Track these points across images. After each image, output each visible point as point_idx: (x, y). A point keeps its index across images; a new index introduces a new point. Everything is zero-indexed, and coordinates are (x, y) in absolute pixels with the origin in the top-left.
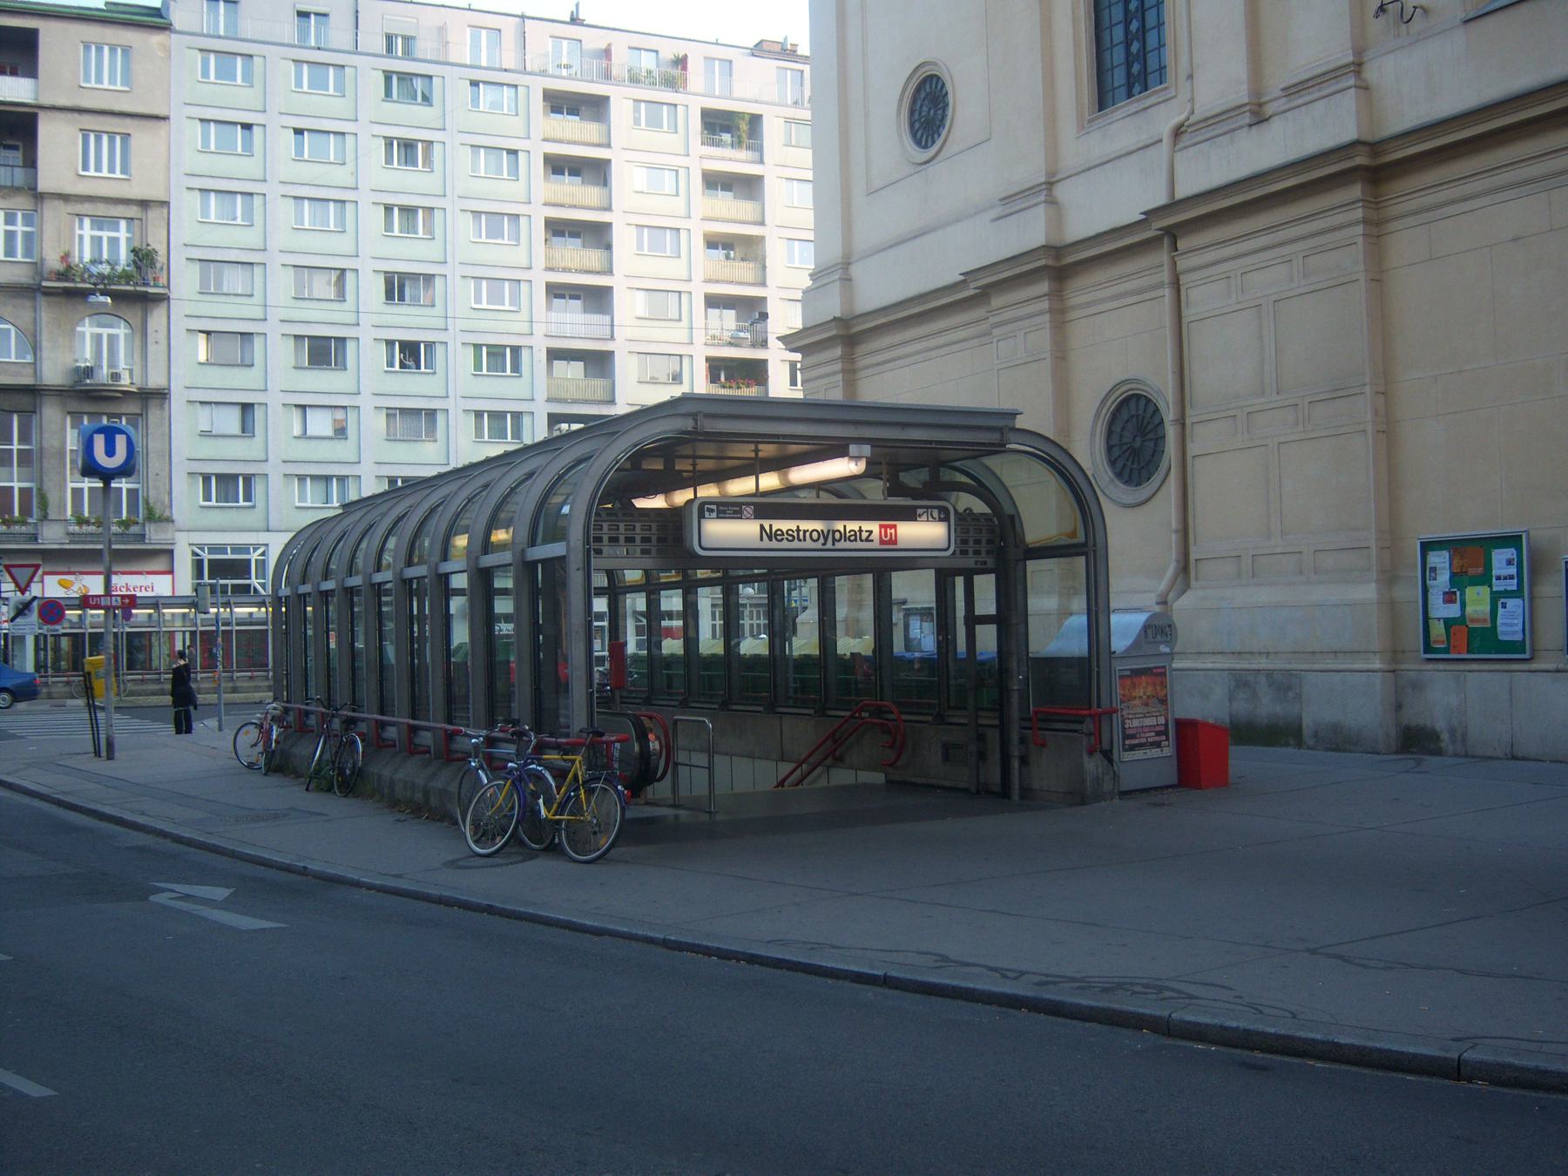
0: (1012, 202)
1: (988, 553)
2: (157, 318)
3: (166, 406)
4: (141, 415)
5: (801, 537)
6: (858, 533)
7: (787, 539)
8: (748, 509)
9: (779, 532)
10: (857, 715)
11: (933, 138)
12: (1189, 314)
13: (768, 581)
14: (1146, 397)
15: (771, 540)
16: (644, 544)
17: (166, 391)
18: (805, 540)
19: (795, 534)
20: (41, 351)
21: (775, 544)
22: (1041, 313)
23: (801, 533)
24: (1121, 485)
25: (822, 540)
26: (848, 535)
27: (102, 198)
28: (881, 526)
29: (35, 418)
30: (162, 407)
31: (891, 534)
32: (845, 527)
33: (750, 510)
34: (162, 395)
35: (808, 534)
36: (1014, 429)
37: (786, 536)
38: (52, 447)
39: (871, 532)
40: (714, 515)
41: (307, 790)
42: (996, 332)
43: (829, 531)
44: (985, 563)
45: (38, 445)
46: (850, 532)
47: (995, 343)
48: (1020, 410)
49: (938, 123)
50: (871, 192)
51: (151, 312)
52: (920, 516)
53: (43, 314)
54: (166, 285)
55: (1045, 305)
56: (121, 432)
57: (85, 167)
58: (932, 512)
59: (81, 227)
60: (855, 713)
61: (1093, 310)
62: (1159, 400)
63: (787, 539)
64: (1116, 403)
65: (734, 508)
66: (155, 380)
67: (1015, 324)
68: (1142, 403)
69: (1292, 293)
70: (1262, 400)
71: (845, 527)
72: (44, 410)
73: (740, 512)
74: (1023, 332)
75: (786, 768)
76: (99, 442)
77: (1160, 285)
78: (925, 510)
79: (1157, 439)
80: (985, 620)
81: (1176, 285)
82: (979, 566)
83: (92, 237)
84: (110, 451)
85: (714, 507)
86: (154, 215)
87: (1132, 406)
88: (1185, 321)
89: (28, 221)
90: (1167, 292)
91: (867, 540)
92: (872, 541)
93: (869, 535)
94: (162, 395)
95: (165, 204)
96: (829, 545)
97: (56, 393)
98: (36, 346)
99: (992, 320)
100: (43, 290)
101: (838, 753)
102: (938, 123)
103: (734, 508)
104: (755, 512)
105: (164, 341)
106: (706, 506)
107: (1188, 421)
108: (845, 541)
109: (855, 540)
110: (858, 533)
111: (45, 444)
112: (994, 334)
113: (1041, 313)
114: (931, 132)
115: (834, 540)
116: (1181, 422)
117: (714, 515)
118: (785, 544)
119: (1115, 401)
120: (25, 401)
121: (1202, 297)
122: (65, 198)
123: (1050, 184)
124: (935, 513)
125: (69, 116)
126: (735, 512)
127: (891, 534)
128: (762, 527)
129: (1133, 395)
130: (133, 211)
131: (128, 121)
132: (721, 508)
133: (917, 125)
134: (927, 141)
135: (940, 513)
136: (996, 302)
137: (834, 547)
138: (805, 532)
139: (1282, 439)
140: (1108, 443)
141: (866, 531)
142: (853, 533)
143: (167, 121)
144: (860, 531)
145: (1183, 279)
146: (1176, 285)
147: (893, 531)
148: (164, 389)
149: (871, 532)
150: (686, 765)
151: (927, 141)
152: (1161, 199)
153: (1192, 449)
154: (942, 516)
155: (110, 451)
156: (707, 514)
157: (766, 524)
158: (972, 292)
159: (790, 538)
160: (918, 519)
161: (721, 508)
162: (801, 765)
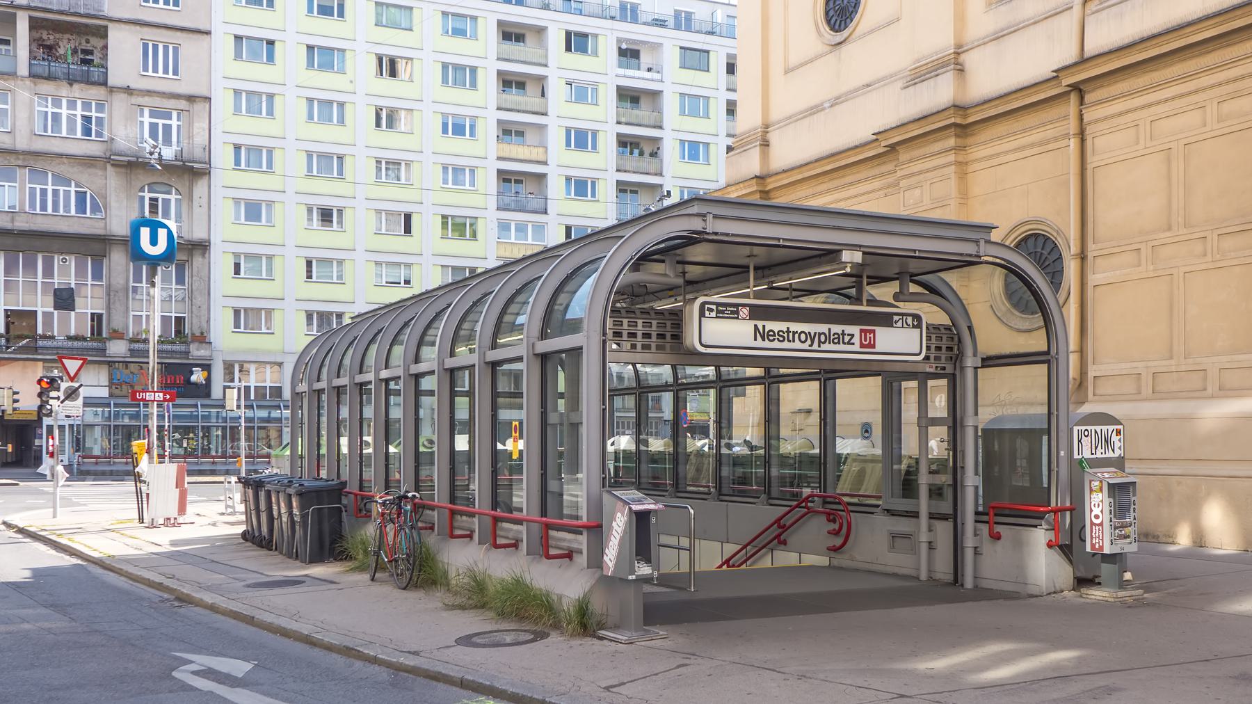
0: (921, 74)
1: (946, 359)
2: (200, 188)
3: (207, 255)
4: (188, 261)
5: (791, 338)
6: (841, 336)
7: (778, 339)
8: (743, 310)
9: (771, 333)
10: (803, 504)
11: (845, 23)
12: (1092, 161)
13: (716, 388)
14: (1043, 235)
15: (764, 340)
16: (659, 340)
17: (207, 244)
18: (794, 341)
19: (786, 335)
20: (110, 210)
21: (767, 344)
22: (947, 165)
23: (791, 335)
24: (1018, 314)
25: (809, 342)
26: (832, 337)
27: (159, 93)
28: (861, 331)
29: (105, 262)
30: (203, 255)
31: (870, 338)
32: (830, 329)
33: (744, 312)
34: (202, 247)
35: (797, 335)
36: (988, 242)
37: (777, 337)
38: (118, 283)
39: (852, 336)
40: (713, 314)
41: (373, 580)
42: (903, 183)
43: (815, 333)
44: (944, 368)
45: (108, 283)
46: (834, 335)
47: (902, 193)
48: (995, 225)
49: (851, 9)
50: (788, 71)
51: (197, 184)
52: (896, 322)
53: (112, 181)
54: (208, 162)
55: (951, 157)
56: (165, 226)
57: (146, 69)
58: (906, 319)
59: (142, 115)
60: (802, 503)
61: (996, 161)
62: (1059, 239)
63: (778, 339)
64: (1016, 241)
65: (732, 309)
66: (198, 234)
67: (922, 176)
68: (1041, 241)
69: (1204, 136)
70: (1168, 234)
71: (830, 329)
72: (112, 255)
73: (737, 312)
74: (929, 183)
75: (730, 549)
76: (145, 233)
77: (1067, 136)
78: (901, 317)
79: (1054, 272)
80: (935, 422)
81: (1082, 135)
82: (939, 371)
83: (151, 124)
84: (154, 242)
85: (714, 307)
86: (199, 107)
87: (1031, 242)
88: (1089, 167)
89: (100, 108)
90: (1073, 143)
91: (849, 343)
92: (853, 344)
93: (850, 339)
94: (202, 247)
95: (208, 99)
96: (815, 347)
97: (122, 242)
98: (106, 205)
99: (899, 174)
100: (112, 162)
101: (782, 537)
102: (851, 9)
103: (732, 309)
104: (750, 312)
105: (205, 205)
106: (707, 306)
107: (1090, 255)
108: (830, 343)
109: (839, 343)
110: (841, 336)
111: (113, 282)
112: (901, 185)
113: (947, 165)
114: (844, 18)
115: (820, 342)
116: (1083, 257)
117: (713, 314)
118: (776, 344)
119: (1015, 239)
120: (96, 247)
121: (1103, 144)
122: (128, 90)
123: (959, 51)
124: (910, 320)
125: (133, 27)
126: (732, 312)
127: (870, 338)
128: (756, 326)
129: (1031, 235)
130: (183, 104)
131: (179, 34)
132: (720, 308)
133: (831, 13)
134: (840, 26)
135: (913, 321)
136: (904, 156)
137: (819, 349)
138: (794, 333)
139: (1188, 269)
140: (1006, 280)
141: (849, 335)
142: (836, 336)
143: (209, 36)
144: (843, 334)
145: (1089, 130)
146: (1082, 135)
147: (872, 335)
148: (206, 242)
149: (852, 336)
150: (676, 548)
151: (840, 26)
152: (1070, 57)
153: (1093, 279)
154: (915, 323)
155: (154, 242)
156: (707, 313)
157: (760, 324)
158: (881, 150)
159: (781, 339)
160: (895, 325)
161: (720, 308)
162: (745, 547)
